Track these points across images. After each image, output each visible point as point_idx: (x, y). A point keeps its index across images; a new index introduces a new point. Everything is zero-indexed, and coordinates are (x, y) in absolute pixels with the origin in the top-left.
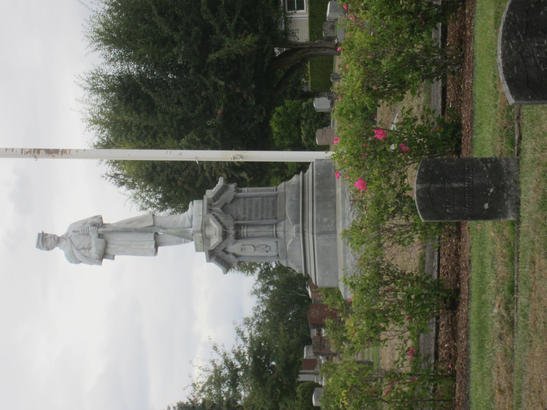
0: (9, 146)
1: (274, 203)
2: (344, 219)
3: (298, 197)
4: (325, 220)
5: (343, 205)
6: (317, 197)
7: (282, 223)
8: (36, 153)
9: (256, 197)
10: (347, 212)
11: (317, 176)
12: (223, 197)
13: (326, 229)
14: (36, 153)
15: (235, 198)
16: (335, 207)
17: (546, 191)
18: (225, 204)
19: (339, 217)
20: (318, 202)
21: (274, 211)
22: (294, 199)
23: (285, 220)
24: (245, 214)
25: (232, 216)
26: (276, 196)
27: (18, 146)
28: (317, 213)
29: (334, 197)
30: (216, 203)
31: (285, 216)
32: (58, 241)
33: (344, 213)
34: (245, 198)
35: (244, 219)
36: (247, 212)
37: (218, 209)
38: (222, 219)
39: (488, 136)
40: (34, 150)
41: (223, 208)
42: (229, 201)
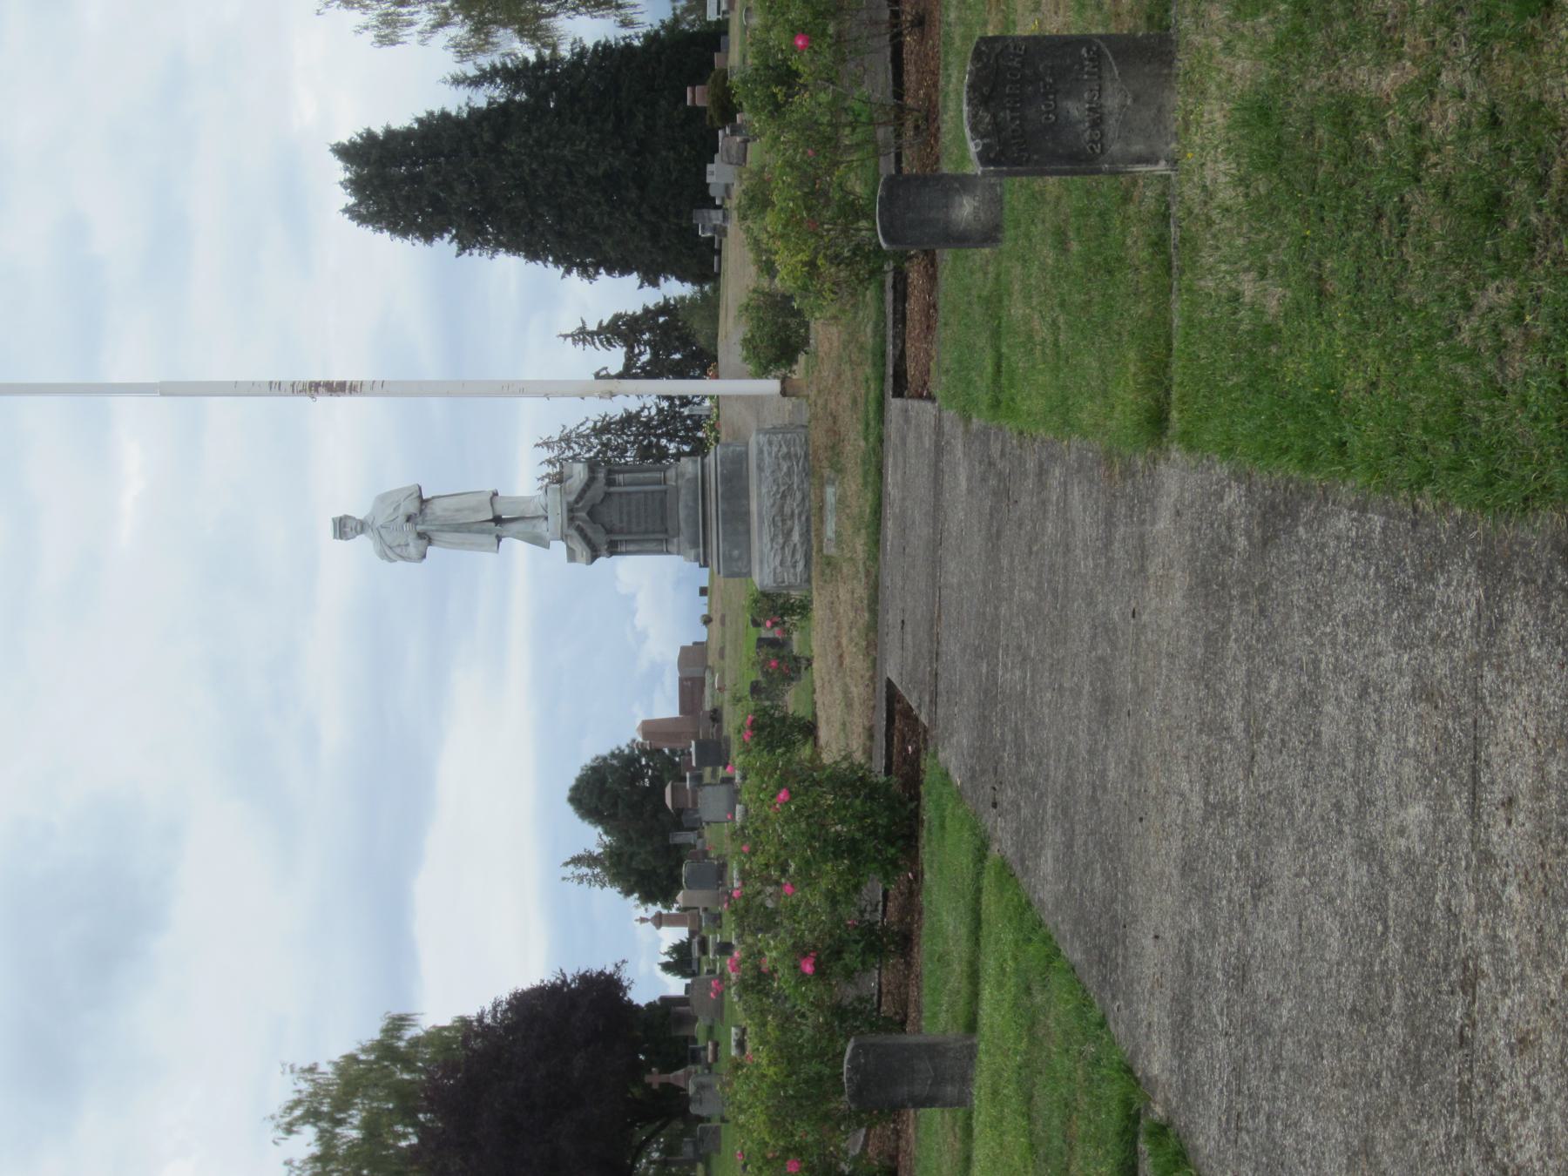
0: (276, 379)
1: (663, 502)
2: (761, 562)
3: (696, 500)
4: (736, 553)
5: (760, 538)
6: (724, 513)
7: (675, 540)
8: (314, 388)
9: (637, 492)
10: (766, 550)
11: (722, 474)
12: (589, 494)
13: (736, 570)
14: (314, 388)
15: (608, 495)
16: (748, 532)
17: (1565, 210)
18: (593, 506)
19: (755, 555)
20: (724, 523)
21: (663, 519)
22: (691, 504)
23: (678, 535)
24: (621, 521)
25: (603, 526)
26: (665, 492)
27: (286, 376)
28: (724, 540)
29: (748, 513)
30: (580, 505)
31: (679, 528)
32: (363, 527)
33: (761, 552)
34: (620, 494)
35: (621, 532)
36: (625, 518)
37: (583, 514)
38: (589, 532)
39: (1220, 171)
40: (311, 384)
41: (590, 514)
42: (598, 500)
